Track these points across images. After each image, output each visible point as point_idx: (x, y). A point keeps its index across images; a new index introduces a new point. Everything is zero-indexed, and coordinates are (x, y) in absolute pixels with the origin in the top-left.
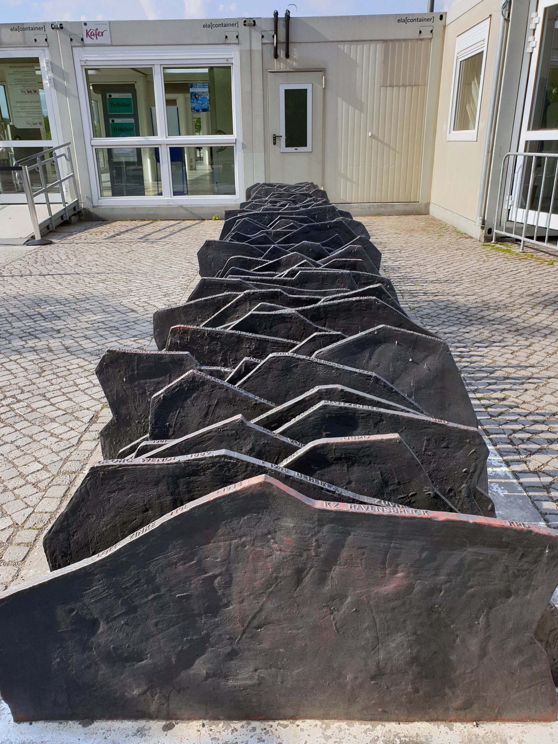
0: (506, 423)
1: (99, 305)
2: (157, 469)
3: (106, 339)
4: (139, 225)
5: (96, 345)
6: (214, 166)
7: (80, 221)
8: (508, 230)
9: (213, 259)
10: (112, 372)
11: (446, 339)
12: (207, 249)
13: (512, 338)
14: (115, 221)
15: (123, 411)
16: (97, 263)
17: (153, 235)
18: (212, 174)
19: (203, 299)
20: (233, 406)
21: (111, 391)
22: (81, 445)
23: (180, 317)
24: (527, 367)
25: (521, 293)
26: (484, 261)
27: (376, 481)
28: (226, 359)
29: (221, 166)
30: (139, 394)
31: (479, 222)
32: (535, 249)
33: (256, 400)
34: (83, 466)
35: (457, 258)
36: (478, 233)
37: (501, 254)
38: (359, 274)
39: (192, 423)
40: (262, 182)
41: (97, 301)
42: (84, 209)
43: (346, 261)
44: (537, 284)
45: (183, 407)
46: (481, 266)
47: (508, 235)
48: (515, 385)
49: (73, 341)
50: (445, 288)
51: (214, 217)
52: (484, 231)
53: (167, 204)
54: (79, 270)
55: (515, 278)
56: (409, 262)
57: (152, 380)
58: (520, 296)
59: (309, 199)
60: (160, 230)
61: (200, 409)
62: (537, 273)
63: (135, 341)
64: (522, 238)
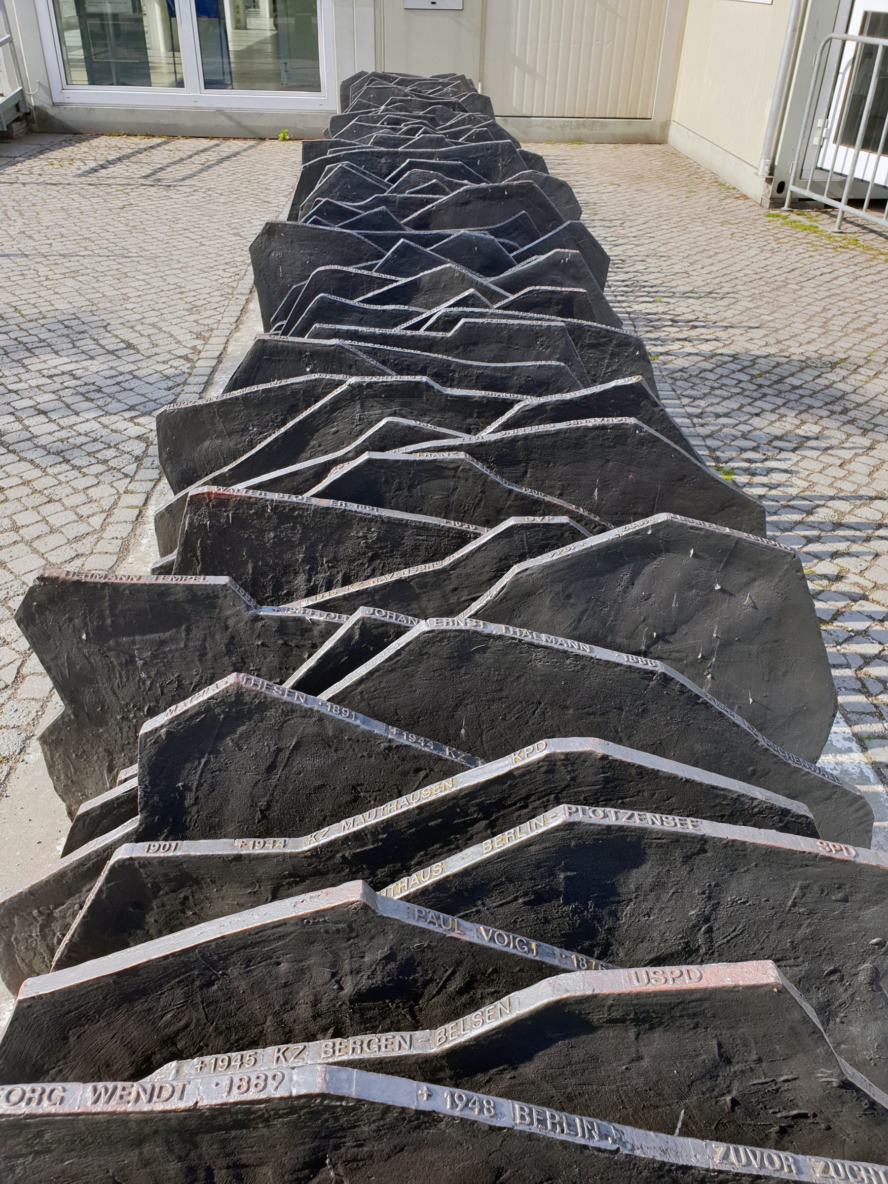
0: (848, 640)
1: (65, 331)
2: (136, 1121)
3: (77, 414)
4: (143, 146)
5: (57, 428)
6: (280, 21)
7: (30, 132)
8: (817, 187)
9: (281, 261)
10: (54, 620)
11: (720, 430)
12: (268, 239)
13: (839, 429)
14: (97, 135)
15: (88, 697)
16: (64, 231)
17: (169, 169)
18: (276, 37)
19: (262, 387)
20: (336, 751)
21: (56, 658)
22: (22, 686)
23: (212, 423)
24: (871, 499)
25: (843, 324)
26: (772, 251)
27: (704, 1057)
28: (315, 558)
29: (292, 21)
30: (120, 664)
31: (764, 170)
32: (859, 226)
33: (390, 741)
34: (24, 742)
35: (724, 243)
36: (758, 188)
37: (801, 235)
38: (580, 327)
39: (240, 783)
40: (370, 70)
41: (61, 322)
42: (35, 107)
43: (553, 292)
44: (871, 303)
45: (215, 752)
46: (767, 262)
47: (815, 196)
48: (854, 542)
49: (12, 418)
50: (708, 311)
51: (281, 135)
52: (771, 187)
53: (193, 105)
54: (27, 246)
55: (830, 289)
56: (639, 249)
57: (148, 637)
58: (842, 331)
59: (460, 116)
60: (182, 160)
61: (256, 755)
62: (869, 279)
63: (132, 419)
64: (842, 206)
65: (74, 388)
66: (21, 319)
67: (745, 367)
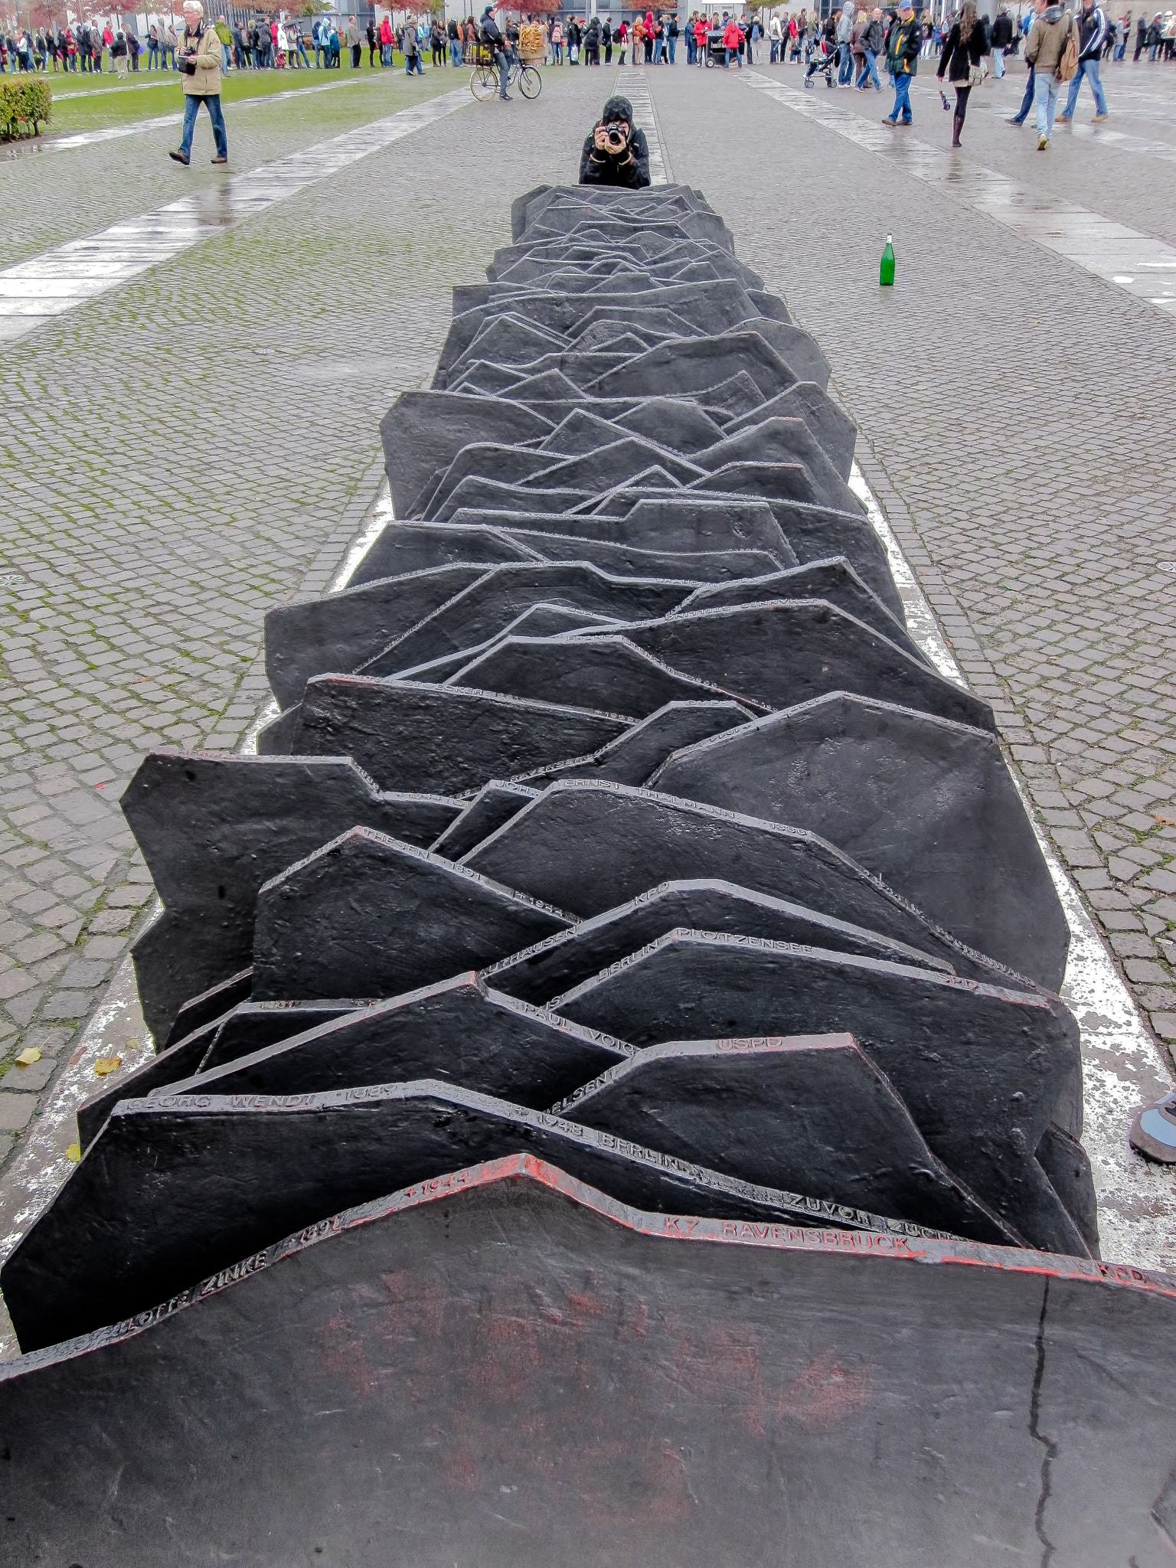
65: (143, 609)
66: (71, 525)
67: (1065, 574)
